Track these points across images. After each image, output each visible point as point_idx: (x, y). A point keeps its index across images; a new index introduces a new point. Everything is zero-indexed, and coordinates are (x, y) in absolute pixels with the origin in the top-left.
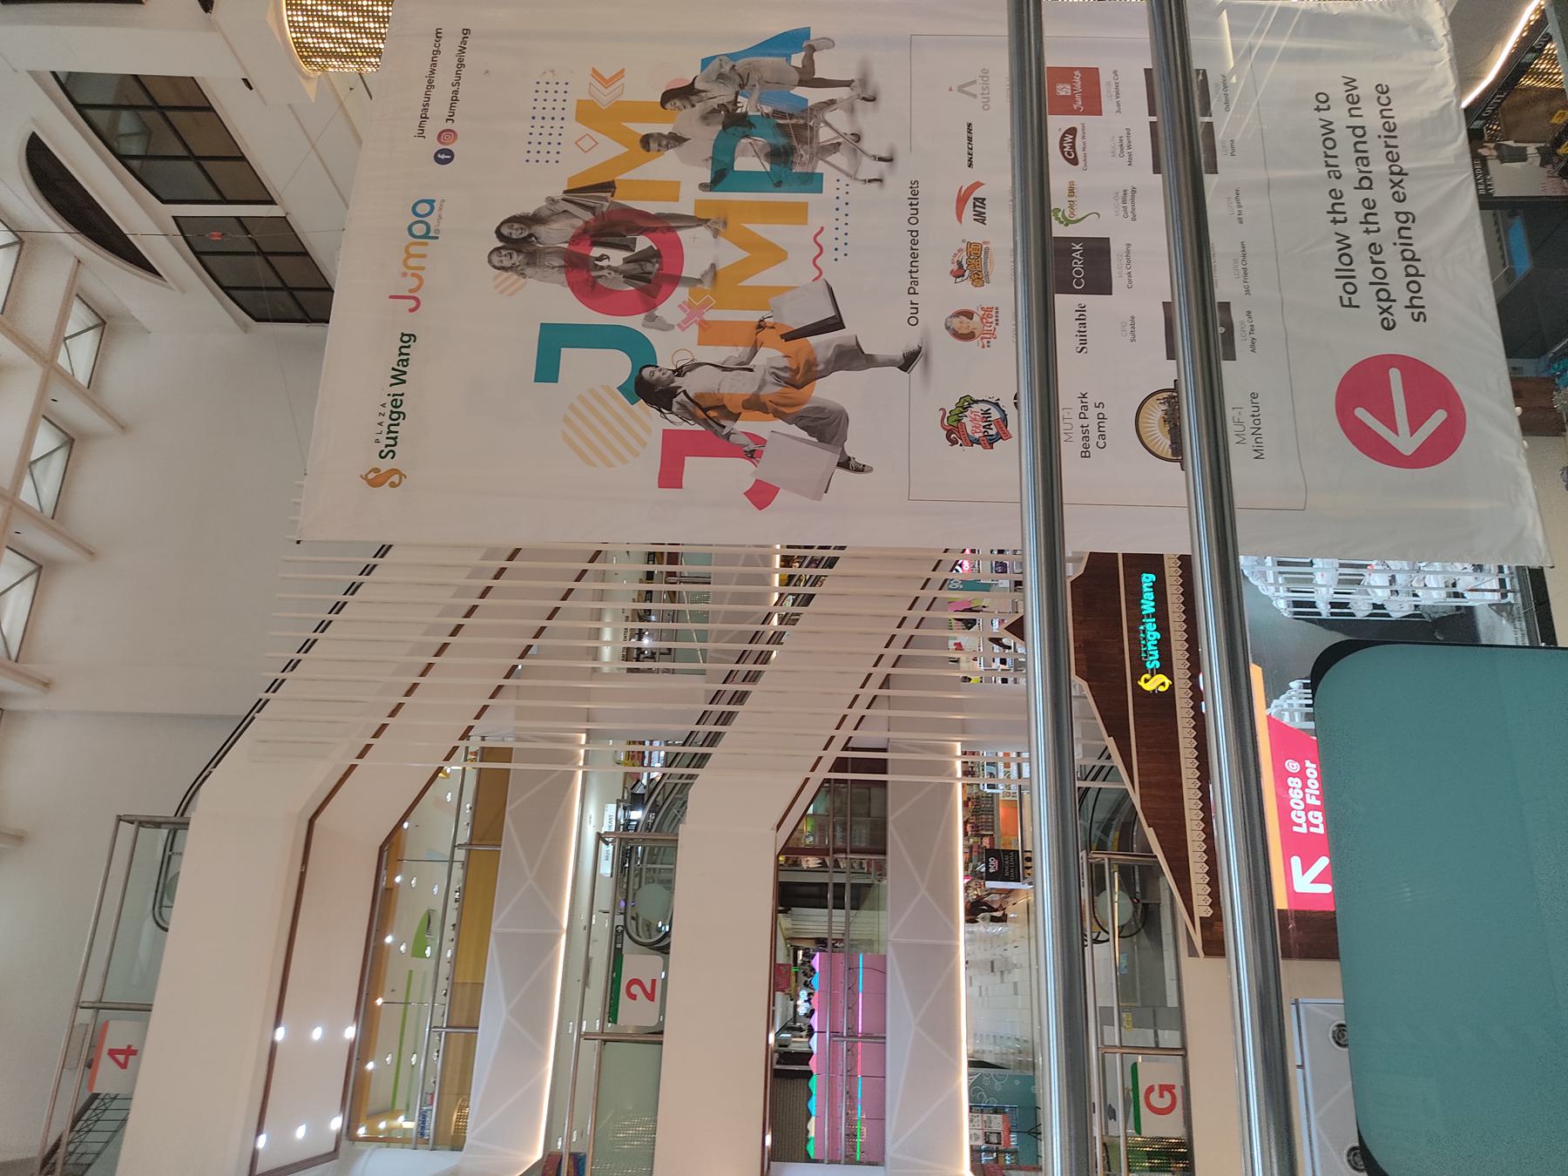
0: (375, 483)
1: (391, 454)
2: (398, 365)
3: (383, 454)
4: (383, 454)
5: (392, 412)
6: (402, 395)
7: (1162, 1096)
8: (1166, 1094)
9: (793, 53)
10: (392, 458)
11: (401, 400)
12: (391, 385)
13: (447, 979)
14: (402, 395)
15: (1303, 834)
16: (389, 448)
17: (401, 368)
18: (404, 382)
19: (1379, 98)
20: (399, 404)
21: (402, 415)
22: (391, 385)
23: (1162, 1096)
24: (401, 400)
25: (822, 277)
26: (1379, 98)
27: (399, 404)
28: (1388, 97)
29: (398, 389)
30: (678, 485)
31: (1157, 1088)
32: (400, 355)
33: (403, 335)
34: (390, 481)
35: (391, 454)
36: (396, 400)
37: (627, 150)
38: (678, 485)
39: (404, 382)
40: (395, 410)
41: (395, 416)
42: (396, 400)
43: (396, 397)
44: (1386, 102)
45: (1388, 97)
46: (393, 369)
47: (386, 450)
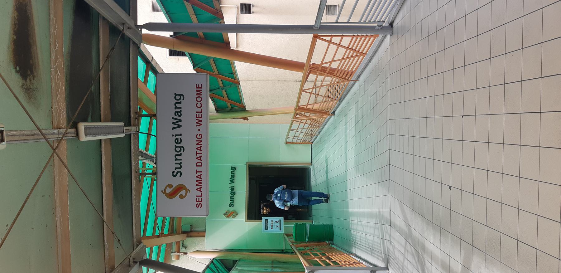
0: (172, 195)
1: (179, 174)
2: (176, 115)
3: (175, 174)
4: (175, 174)
5: (176, 147)
6: (181, 135)
7: (199, 136)
8: (200, 136)
9: (380, 34)
10: (180, 176)
11: (181, 139)
12: (173, 129)
13: (198, 233)
14: (181, 135)
15: (282, 209)
16: (178, 170)
17: (177, 117)
18: (180, 126)
19: (197, 104)
20: (179, 141)
21: (182, 148)
22: (173, 129)
23: (199, 136)
24: (181, 139)
25: (201, 108)
26: (197, 104)
27: (179, 141)
28: (201, 104)
29: (177, 131)
30: (181, 107)
31: (198, 135)
32: (175, 109)
33: (176, 95)
34: (179, 194)
35: (179, 174)
36: (177, 139)
37: (143, 110)
38: (181, 107)
39: (180, 126)
40: (177, 145)
41: (178, 149)
42: (177, 139)
43: (177, 137)
44: (200, 105)
45: (201, 104)
46: (173, 118)
47: (176, 171)
